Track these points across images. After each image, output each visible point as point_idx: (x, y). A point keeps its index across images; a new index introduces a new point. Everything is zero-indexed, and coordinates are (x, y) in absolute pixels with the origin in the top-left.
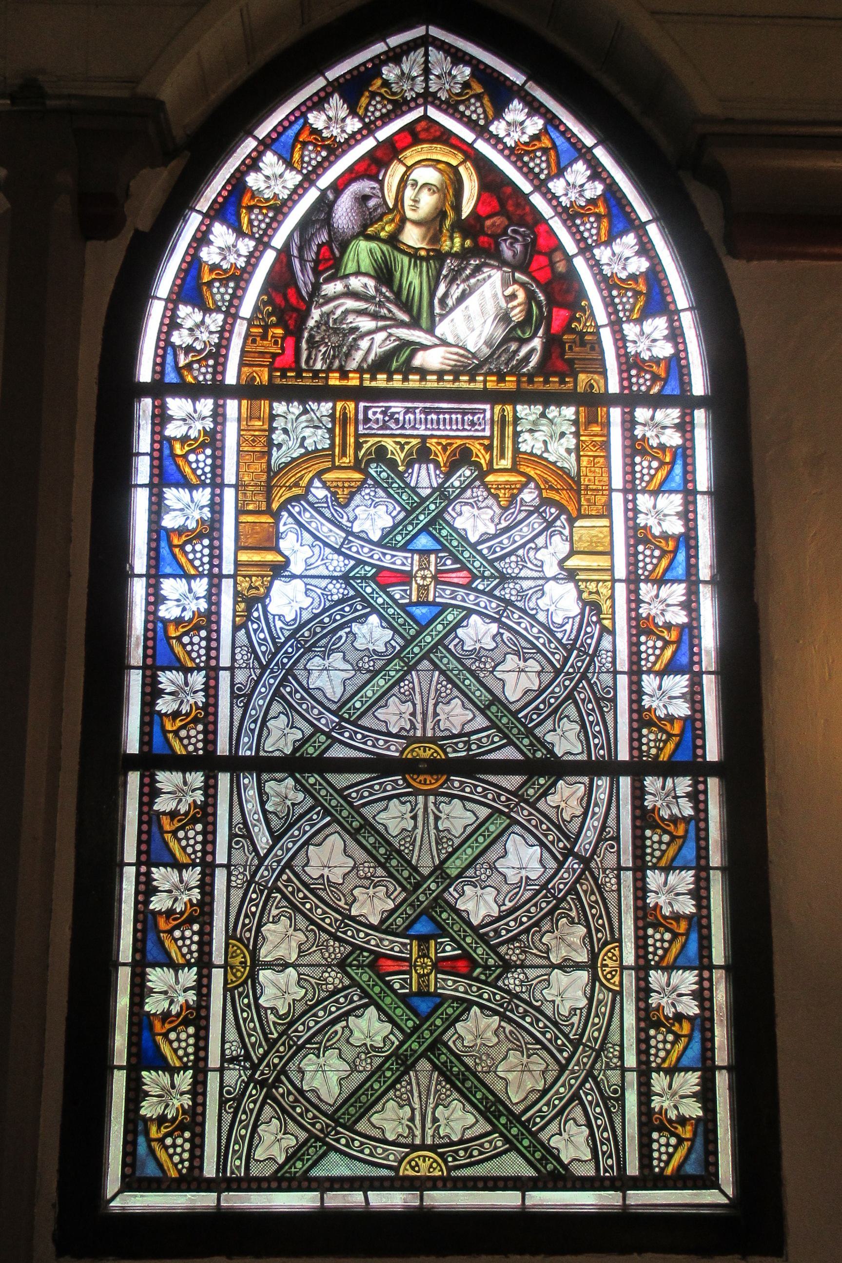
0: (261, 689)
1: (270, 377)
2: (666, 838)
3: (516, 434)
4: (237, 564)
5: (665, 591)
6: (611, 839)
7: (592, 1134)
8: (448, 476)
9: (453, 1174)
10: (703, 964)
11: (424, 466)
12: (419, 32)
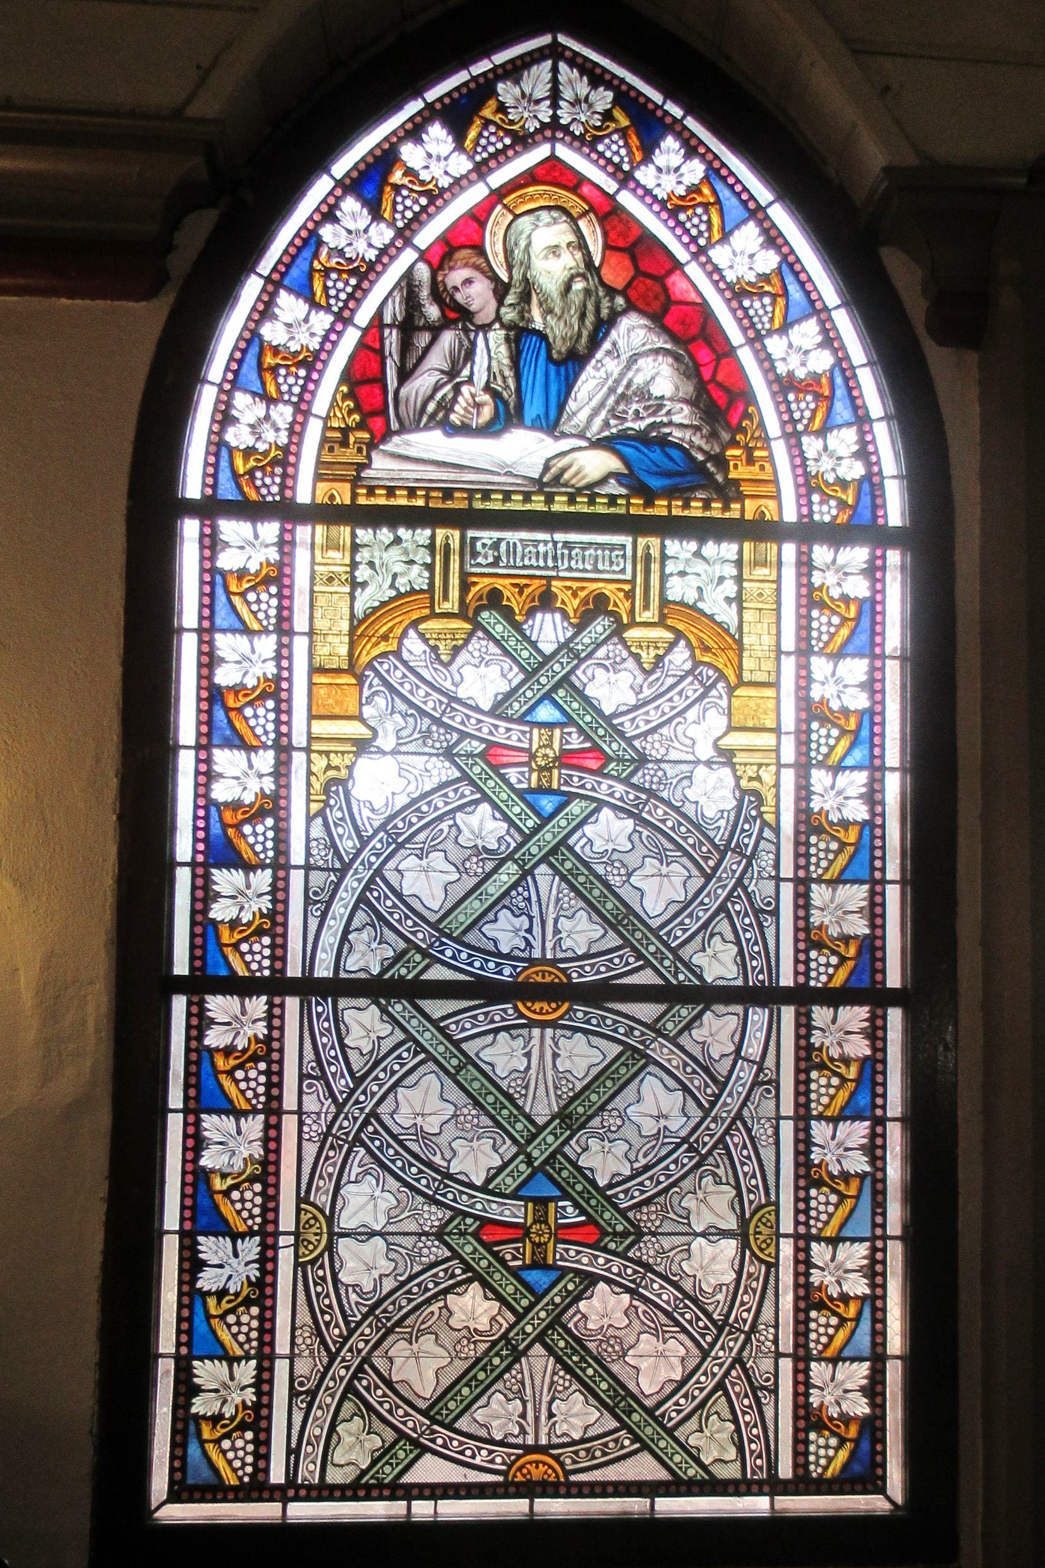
0: (341, 893)
1: (354, 496)
2: (834, 1321)
3: (663, 578)
4: (311, 738)
5: (842, 780)
6: (769, 1082)
7: (741, 952)
8: (580, 628)
9: (573, 1478)
10: (874, 654)
11: (548, 616)
12: (545, 40)
